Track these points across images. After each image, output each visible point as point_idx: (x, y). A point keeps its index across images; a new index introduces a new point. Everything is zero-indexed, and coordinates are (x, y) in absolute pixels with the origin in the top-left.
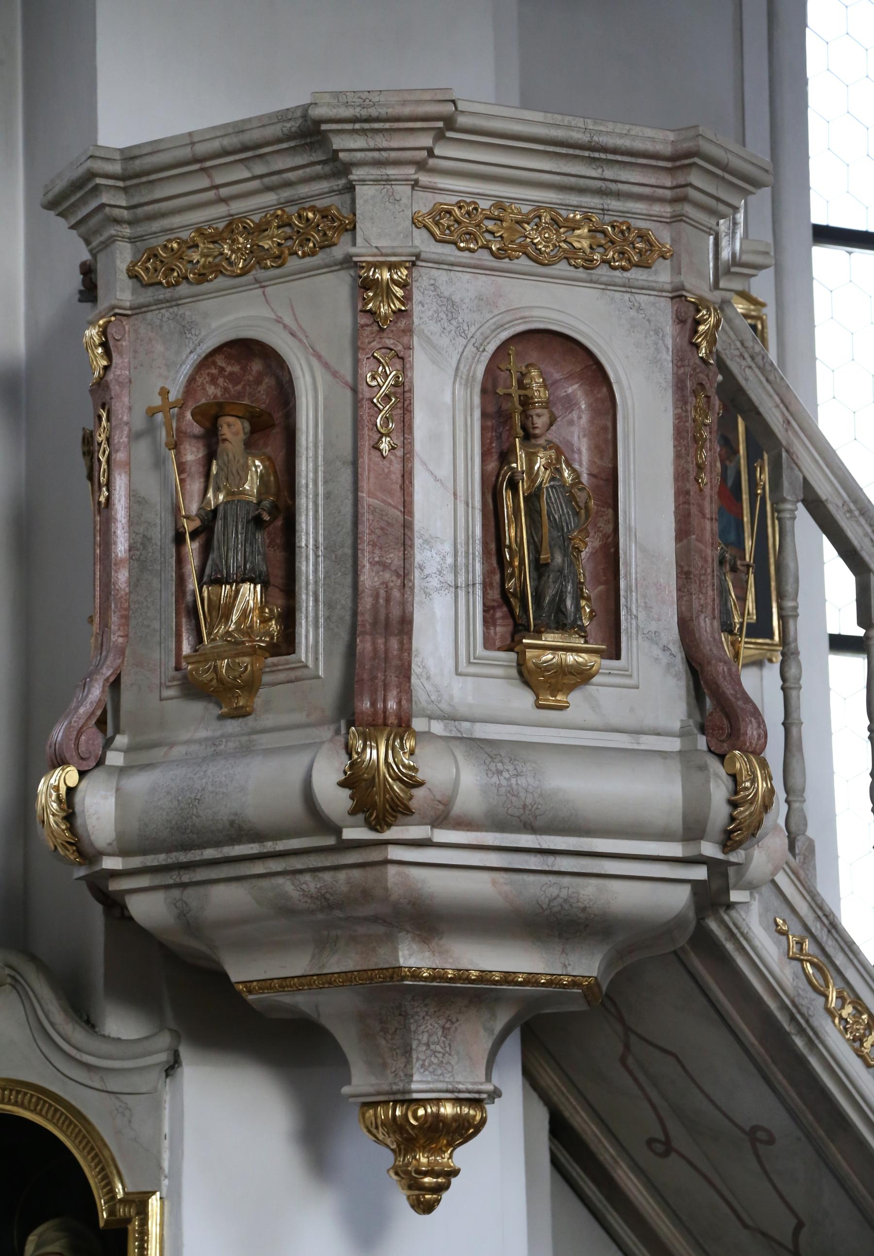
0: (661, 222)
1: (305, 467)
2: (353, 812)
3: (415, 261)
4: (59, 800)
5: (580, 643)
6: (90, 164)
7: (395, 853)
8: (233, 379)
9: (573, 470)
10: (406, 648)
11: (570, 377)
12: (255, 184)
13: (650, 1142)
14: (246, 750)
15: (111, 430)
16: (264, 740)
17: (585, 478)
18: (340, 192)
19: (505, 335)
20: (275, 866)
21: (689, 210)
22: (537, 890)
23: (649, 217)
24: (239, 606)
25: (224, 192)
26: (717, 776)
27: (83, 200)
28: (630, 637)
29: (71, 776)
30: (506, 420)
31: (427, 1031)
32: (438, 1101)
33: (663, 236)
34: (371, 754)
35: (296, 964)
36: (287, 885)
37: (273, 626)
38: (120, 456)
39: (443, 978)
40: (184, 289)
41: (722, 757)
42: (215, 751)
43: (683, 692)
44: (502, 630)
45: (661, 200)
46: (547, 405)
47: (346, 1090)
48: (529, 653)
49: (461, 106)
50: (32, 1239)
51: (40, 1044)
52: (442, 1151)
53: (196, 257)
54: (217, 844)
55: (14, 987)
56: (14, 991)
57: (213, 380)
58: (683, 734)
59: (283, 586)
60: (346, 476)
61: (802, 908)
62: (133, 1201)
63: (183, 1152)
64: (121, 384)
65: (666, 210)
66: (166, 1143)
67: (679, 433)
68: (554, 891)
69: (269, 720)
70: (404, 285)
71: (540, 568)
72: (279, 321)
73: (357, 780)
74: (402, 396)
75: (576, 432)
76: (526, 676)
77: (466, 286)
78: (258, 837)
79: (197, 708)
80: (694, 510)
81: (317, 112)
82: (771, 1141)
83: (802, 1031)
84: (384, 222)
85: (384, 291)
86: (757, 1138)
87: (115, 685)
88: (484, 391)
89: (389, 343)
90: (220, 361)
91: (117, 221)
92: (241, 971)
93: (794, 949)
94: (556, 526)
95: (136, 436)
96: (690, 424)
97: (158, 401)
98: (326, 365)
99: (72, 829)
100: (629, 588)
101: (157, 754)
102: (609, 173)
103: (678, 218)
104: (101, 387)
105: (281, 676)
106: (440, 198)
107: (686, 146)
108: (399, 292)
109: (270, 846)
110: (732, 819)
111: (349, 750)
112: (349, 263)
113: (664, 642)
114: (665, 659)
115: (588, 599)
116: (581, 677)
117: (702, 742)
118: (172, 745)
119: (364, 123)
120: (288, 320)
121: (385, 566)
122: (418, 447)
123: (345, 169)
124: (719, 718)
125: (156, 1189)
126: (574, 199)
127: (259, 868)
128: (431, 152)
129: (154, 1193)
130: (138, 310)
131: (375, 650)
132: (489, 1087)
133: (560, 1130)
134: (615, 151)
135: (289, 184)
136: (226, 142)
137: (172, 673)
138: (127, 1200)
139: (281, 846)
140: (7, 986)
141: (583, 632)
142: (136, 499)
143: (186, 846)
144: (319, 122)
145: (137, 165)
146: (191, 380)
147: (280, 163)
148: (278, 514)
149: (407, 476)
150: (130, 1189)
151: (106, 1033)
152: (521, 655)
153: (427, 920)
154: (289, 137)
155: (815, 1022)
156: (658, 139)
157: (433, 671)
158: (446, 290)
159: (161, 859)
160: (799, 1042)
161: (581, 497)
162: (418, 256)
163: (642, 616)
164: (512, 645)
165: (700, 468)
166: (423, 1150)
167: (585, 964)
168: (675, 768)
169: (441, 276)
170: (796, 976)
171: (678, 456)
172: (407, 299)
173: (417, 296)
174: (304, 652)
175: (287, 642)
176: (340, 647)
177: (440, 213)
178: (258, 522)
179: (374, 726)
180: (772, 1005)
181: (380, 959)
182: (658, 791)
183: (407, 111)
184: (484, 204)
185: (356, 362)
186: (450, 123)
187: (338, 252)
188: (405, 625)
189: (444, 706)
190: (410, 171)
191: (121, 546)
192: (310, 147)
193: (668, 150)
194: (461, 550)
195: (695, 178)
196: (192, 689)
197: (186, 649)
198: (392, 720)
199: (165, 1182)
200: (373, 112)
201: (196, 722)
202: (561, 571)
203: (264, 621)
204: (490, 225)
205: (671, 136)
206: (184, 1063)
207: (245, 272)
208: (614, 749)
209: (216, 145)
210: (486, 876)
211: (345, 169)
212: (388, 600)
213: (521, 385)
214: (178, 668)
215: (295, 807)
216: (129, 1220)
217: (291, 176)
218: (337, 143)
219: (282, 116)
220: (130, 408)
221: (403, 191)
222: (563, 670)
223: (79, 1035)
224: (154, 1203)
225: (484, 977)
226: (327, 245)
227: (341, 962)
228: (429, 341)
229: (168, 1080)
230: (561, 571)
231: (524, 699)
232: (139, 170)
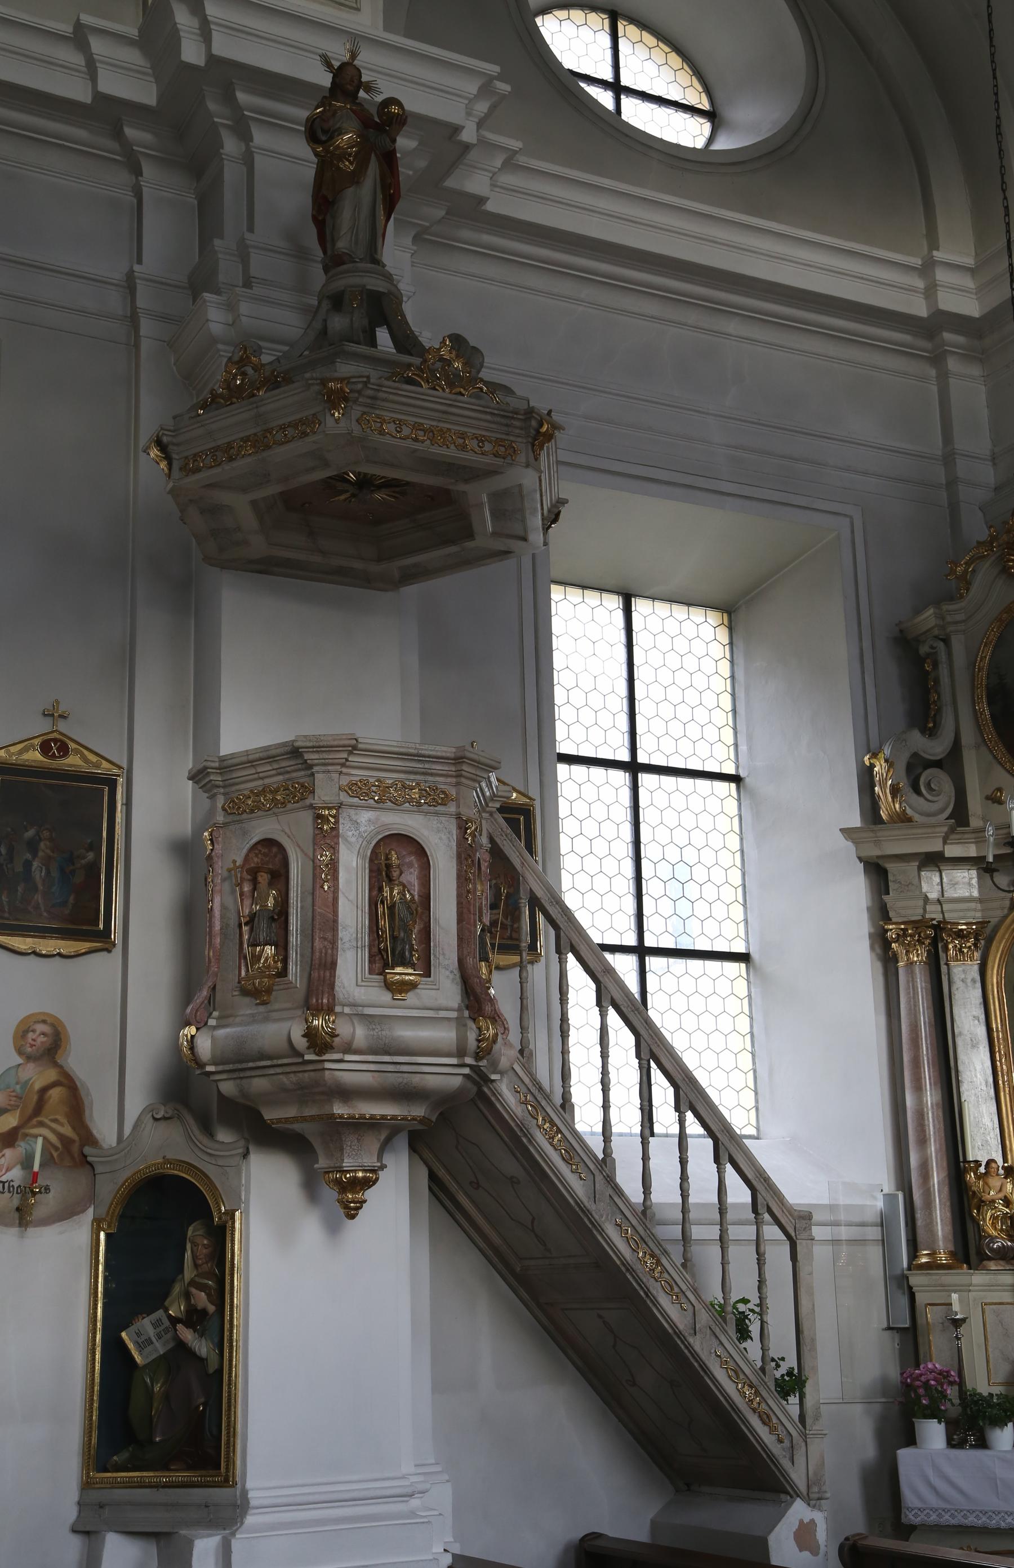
0: (853, 532)
1: (292, 894)
2: (308, 1048)
3: (340, 806)
4: (187, 1041)
5: (410, 971)
6: (205, 764)
7: (328, 1065)
8: (265, 855)
9: (411, 894)
10: (333, 975)
11: (410, 853)
12: (274, 772)
13: (471, 1183)
14: (266, 1019)
15: (213, 877)
16: (275, 1015)
17: (416, 897)
18: (309, 776)
19: (380, 837)
20: (279, 1070)
21: (463, 780)
22: (393, 1079)
23: (445, 783)
24: (265, 955)
25: (261, 775)
26: (471, 1029)
27: (204, 778)
28: (435, 967)
29: (193, 1030)
30: (381, 872)
31: (350, 1141)
32: (355, 1171)
33: (453, 792)
34: (316, 1022)
35: (291, 1112)
36: (284, 1079)
37: (279, 965)
38: (217, 888)
39: (353, 1118)
40: (245, 816)
41: (474, 1020)
42: (253, 1020)
43: (459, 991)
44: (378, 965)
45: (451, 776)
46: (398, 866)
47: (316, 1166)
48: (388, 976)
49: (360, 740)
50: (191, 1229)
52: (358, 1193)
53: (250, 802)
54: (253, 1061)
57: (257, 855)
58: (459, 1010)
59: (283, 946)
60: (309, 899)
61: (527, 1080)
64: (218, 857)
65: (454, 780)
67: (459, 877)
68: (400, 1080)
69: (276, 1006)
70: (334, 817)
71: (394, 938)
72: (283, 831)
73: (310, 1034)
74: (333, 866)
75: (411, 877)
76: (388, 986)
77: (365, 817)
78: (270, 1058)
79: (247, 1000)
80: (465, 911)
81: (297, 744)
82: (519, 1182)
83: (525, 1135)
84: (326, 789)
85: (325, 819)
86: (513, 1181)
87: (214, 988)
88: (371, 860)
89: (328, 841)
90: (259, 847)
91: (218, 787)
92: (269, 1115)
93: (523, 1099)
94: (401, 920)
95: (224, 880)
96: (463, 873)
97: (232, 866)
98: (302, 850)
99: (193, 1053)
100: (435, 945)
101: (231, 1019)
102: (426, 766)
103: (458, 784)
104: (210, 857)
105: (282, 987)
106: (353, 778)
107: (459, 754)
108: (333, 820)
109: (275, 1062)
110: (479, 1047)
111: (307, 1021)
112: (311, 807)
113: (451, 969)
114: (451, 976)
115: (417, 951)
116: (412, 986)
117: (466, 1013)
118: (236, 1016)
119: (318, 748)
120: (287, 830)
121: (325, 939)
122: (340, 886)
123: (310, 767)
124: (475, 1000)
126: (412, 777)
127: (272, 1071)
128: (347, 760)
130: (226, 825)
131: (319, 976)
132: (379, 1164)
133: (433, 1177)
134: (429, 757)
135: (288, 772)
136: (261, 755)
137: (237, 985)
138: (226, 1213)
139: (280, 1062)
141: (413, 966)
142: (224, 907)
143: (240, 1060)
144: (299, 748)
145: (225, 763)
146: (247, 855)
147: (284, 764)
148: (281, 913)
149: (335, 900)
152: (385, 977)
153: (346, 1094)
154: (287, 753)
155: (531, 1131)
156: (448, 751)
157: (346, 984)
158: (354, 817)
159: (231, 1067)
160: (525, 1140)
161: (413, 906)
162: (341, 804)
163: (441, 958)
164: (382, 973)
165: (468, 892)
166: (349, 1194)
167: (419, 1111)
168: (454, 1025)
169: (352, 812)
170: (523, 1111)
171: (458, 887)
172: (337, 822)
173: (341, 821)
174: (291, 977)
175: (283, 973)
176: (306, 975)
177: (352, 784)
178: (273, 919)
179: (317, 1010)
180: (513, 1124)
181: (325, 1110)
182: (445, 1035)
183: (336, 743)
184: (371, 780)
185: (314, 850)
186: (355, 747)
187: (308, 802)
188: (334, 965)
189: (351, 1000)
190: (338, 767)
191: (217, 927)
192: (296, 757)
193: (452, 756)
194: (360, 931)
195: (465, 767)
196: (245, 992)
197: (243, 973)
198: (325, 1008)
200: (321, 744)
201: (246, 1007)
202: (403, 940)
203: (275, 962)
204: (374, 788)
205: (454, 750)
207: (269, 809)
208: (425, 1019)
209: (257, 756)
210: (369, 1074)
211: (310, 767)
212: (326, 954)
213: (387, 859)
214: (239, 982)
215: (285, 1045)
216: (227, 1222)
217: (288, 769)
218: (306, 756)
219: (284, 744)
220: (221, 868)
221: (335, 776)
222: (403, 983)
223: (205, 1140)
225: (373, 1117)
226: (303, 799)
227: (310, 1111)
228: (346, 840)
230: (403, 940)
231: (386, 997)
232: (227, 766)
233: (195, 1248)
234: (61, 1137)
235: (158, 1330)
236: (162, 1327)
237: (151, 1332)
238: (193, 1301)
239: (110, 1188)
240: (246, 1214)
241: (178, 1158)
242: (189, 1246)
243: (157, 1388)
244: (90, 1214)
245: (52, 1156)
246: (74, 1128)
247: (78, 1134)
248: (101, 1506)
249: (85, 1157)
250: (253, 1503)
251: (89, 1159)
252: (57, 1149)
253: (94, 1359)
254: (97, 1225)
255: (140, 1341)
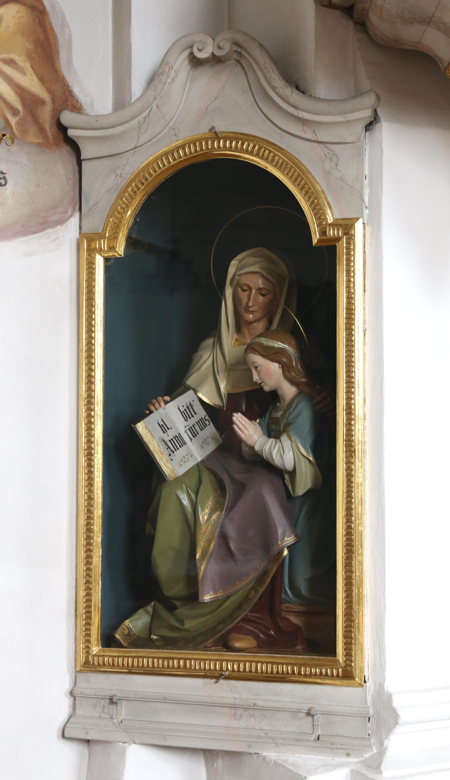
51: (261, 105)
55: (238, 62)
56: (238, 66)
62: (341, 225)
63: (382, 188)
66: (366, 182)
125: (359, 216)
129: (358, 219)
138: (335, 225)
140: (233, 61)
150: (338, 216)
151: (317, 96)
199: (366, 212)
206: (382, 119)
216: (338, 239)
224: (359, 226)
229: (367, 134)
233: (244, 296)
234: (21, 92)
235: (192, 421)
236: (196, 418)
237: (180, 425)
238: (256, 377)
239: (118, 177)
240: (375, 223)
241: (231, 130)
242: (229, 292)
243: (203, 516)
244: (71, 229)
245: (7, 122)
246: (42, 79)
247: (50, 91)
248: (112, 701)
249: (62, 129)
250: (404, 715)
251: (71, 133)
252: (15, 112)
253: (90, 466)
254: (88, 242)
255: (167, 439)
